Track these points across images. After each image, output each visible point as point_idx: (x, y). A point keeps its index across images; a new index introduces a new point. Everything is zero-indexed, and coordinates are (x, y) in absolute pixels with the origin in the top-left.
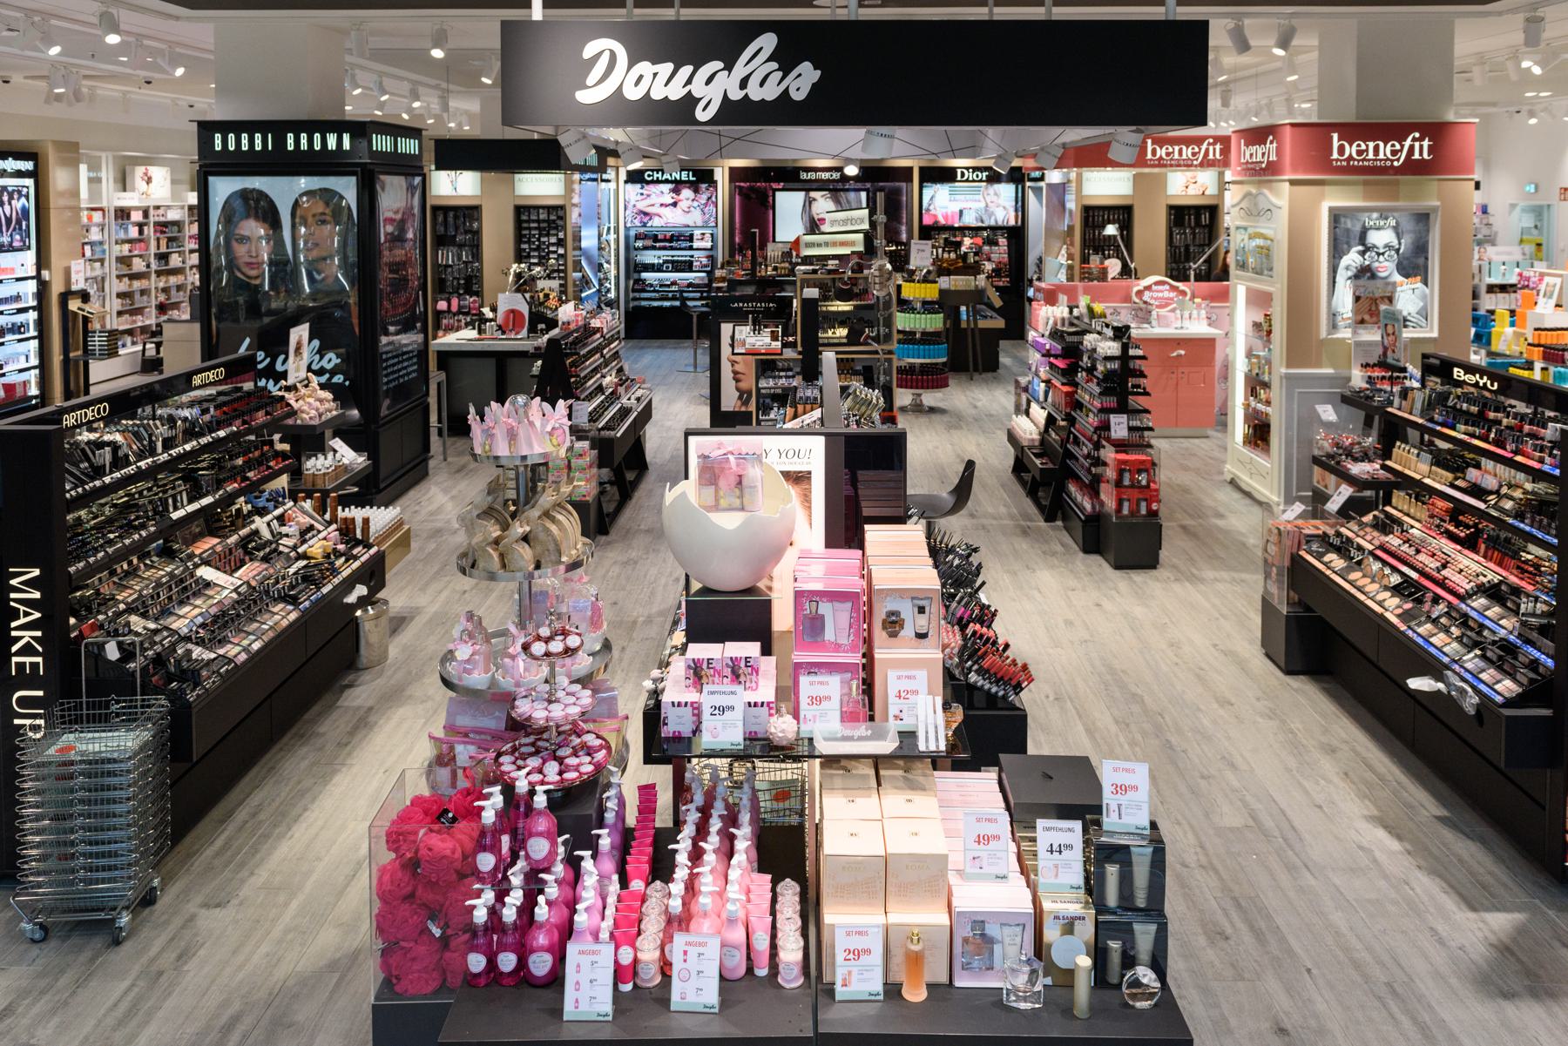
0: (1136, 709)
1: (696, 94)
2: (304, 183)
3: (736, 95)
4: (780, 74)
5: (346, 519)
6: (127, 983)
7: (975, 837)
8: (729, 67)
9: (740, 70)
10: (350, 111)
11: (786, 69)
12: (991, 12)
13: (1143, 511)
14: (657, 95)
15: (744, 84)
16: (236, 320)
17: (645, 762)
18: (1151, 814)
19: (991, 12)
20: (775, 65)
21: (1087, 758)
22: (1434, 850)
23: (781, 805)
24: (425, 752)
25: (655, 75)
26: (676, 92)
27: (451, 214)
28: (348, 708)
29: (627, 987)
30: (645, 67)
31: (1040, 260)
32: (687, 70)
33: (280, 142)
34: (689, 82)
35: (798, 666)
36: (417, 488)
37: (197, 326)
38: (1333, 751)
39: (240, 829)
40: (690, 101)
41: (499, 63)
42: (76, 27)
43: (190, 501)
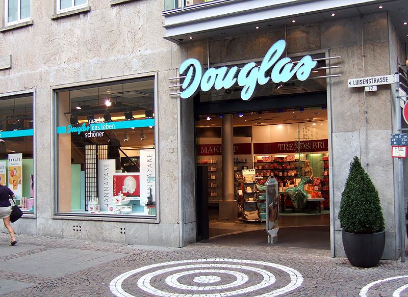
1: (240, 84)
3: (263, 81)
4: (291, 65)
5: (282, 195)
8: (259, 64)
9: (265, 65)
11: (295, 59)
13: (396, 143)
14: (218, 87)
15: (268, 73)
16: (288, 186)
20: (287, 60)
25: (217, 75)
26: (228, 84)
27: (204, 141)
30: (212, 71)
32: (234, 70)
34: (236, 76)
40: (237, 89)
42: (254, 262)
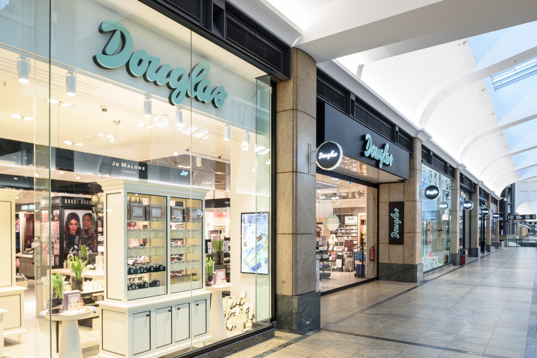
43: (480, 200)
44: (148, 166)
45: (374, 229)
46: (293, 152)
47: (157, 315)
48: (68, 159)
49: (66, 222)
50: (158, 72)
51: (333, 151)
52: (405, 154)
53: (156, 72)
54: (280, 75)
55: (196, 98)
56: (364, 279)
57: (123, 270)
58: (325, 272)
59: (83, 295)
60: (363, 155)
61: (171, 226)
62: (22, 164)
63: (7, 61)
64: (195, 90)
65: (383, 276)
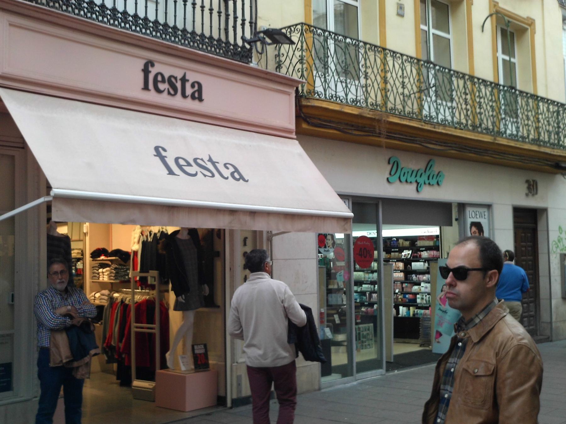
0: (299, 27)
2: (437, 130)
6: (106, 258)
7: (399, 19)
10: (209, 353)
12: (379, 232)
17: (452, 226)
18: (336, 192)
19: (379, 232)
21: (310, 309)
22: (511, 156)
23: (458, 380)
24: (319, 91)
28: (297, 356)
29: (488, 83)
31: (425, 172)
33: (376, 260)
35: (428, 273)
36: (68, 344)
37: (54, 218)
38: (142, 235)
39: (220, 29)
41: (549, 152)
43: (504, 60)
44: (302, 402)
45: (421, 18)
46: (330, 122)
47: (187, 410)
48: (23, 148)
49: (54, 406)
50: (13, 29)
51: (169, 233)
52: (424, 5)
53: (483, 31)
54: (292, 405)
55: (429, 184)
56: (18, 399)
57: (146, 92)
58: (372, 234)
59: (559, 236)
60: (221, 401)
61: (155, 281)
62: (193, 232)
63: (239, 22)
64: (428, 179)
65: (303, 338)
